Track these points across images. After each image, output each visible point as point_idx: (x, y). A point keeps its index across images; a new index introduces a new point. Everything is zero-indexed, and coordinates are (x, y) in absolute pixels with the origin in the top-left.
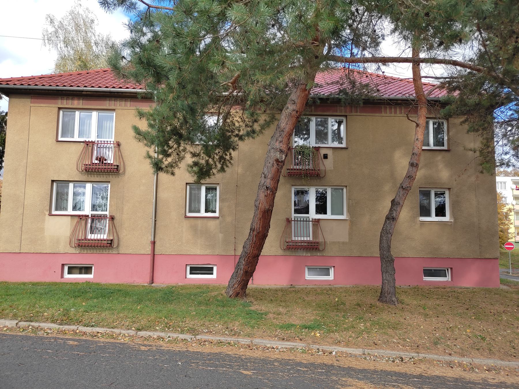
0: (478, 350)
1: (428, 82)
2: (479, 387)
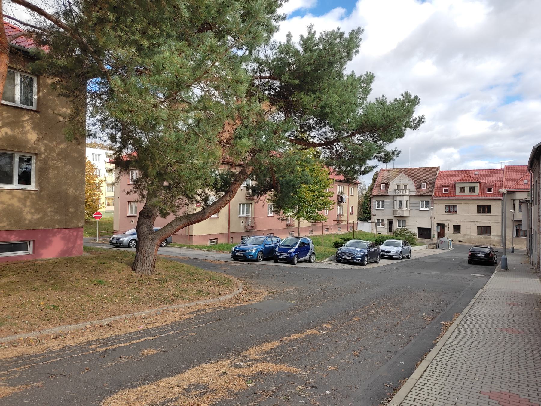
0: (48, 320)
1: (7, 21)
2: (41, 358)
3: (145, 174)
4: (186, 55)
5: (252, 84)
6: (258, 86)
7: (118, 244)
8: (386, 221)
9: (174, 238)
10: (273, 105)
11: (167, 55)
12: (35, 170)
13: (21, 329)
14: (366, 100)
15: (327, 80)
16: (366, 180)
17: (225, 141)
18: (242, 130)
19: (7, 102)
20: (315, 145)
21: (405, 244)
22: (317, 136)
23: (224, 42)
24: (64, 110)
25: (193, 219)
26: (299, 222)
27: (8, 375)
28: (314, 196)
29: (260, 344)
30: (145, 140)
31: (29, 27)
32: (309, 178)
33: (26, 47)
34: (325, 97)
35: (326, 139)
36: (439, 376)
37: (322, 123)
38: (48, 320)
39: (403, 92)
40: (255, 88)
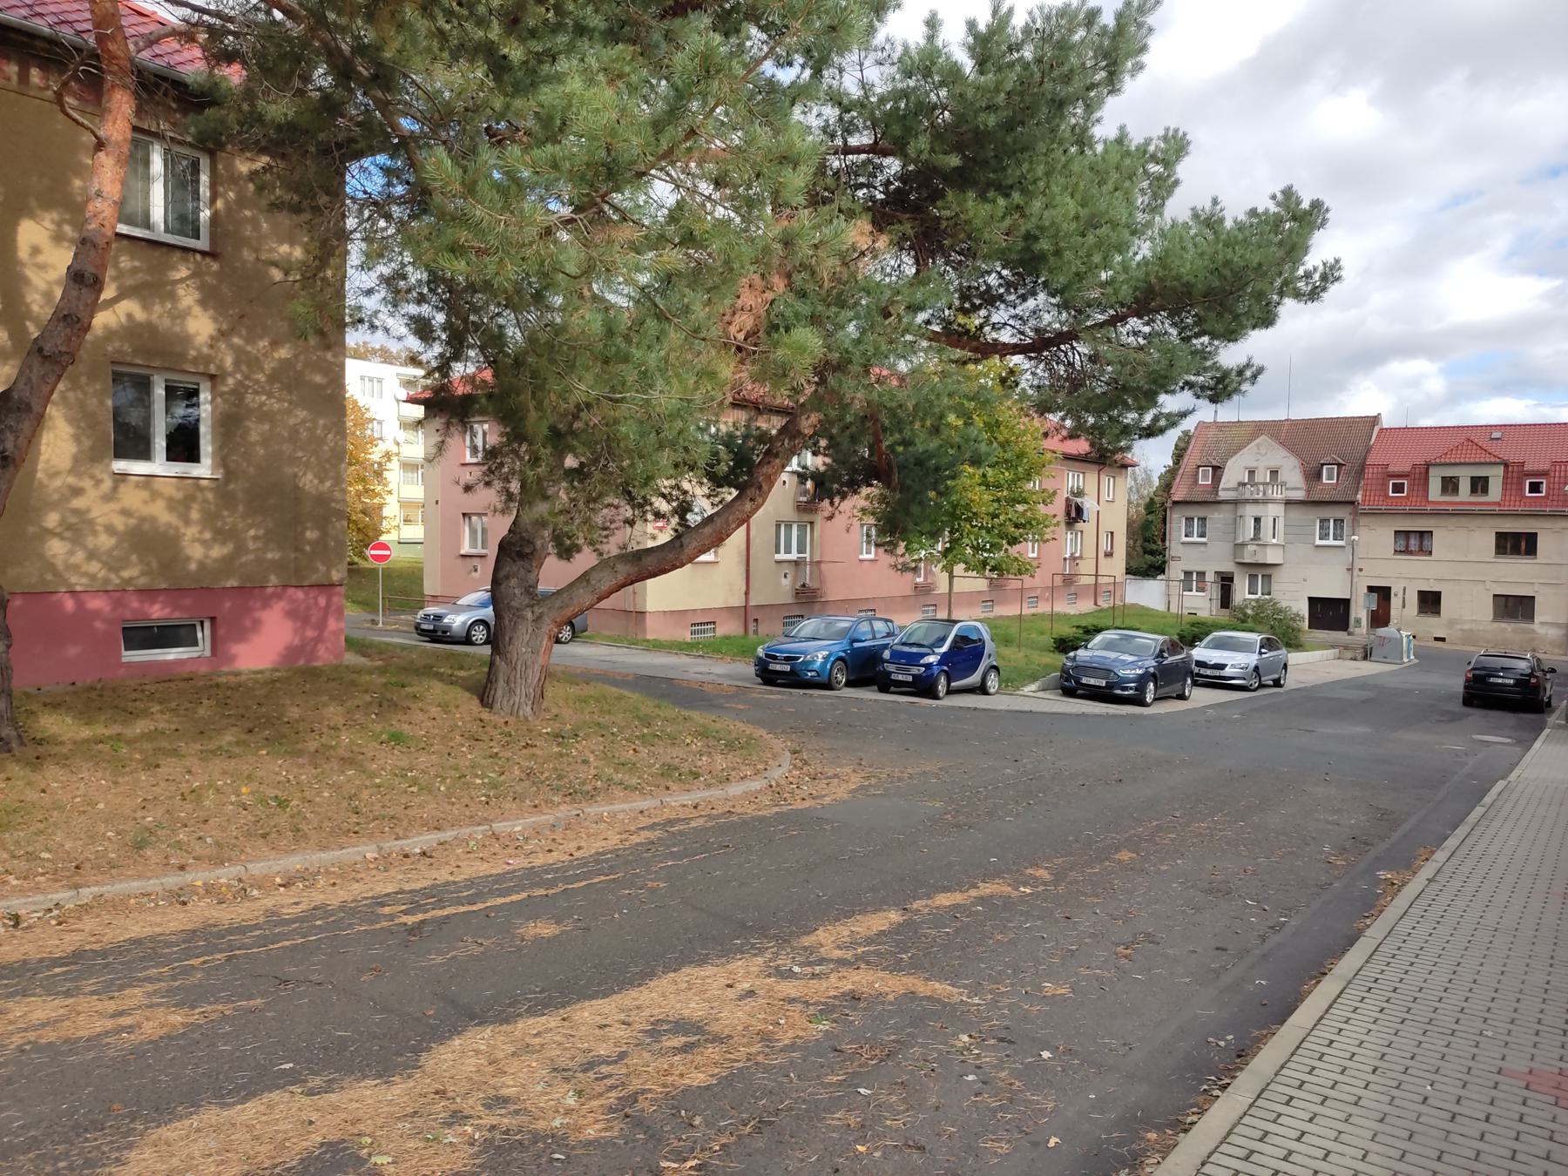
0: (264, 836)
3: (516, 433)
4: (629, 85)
5: (822, 168)
6: (837, 173)
7: (437, 634)
8: (1210, 577)
9: (592, 619)
10: (881, 230)
11: (575, 84)
12: (210, 423)
13: (194, 858)
14: (1161, 215)
15: (1045, 155)
16: (1152, 456)
17: (741, 336)
18: (790, 306)
19: (131, 228)
20: (1005, 350)
21: (1268, 644)
22: (1011, 322)
23: (738, 45)
24: (285, 249)
25: (649, 562)
26: (951, 577)
27: (174, 978)
28: (998, 500)
29: (845, 917)
30: (514, 333)
31: (189, 11)
32: (983, 448)
33: (179, 68)
34: (1037, 205)
35: (1037, 330)
36: (1374, 1022)
37: (1025, 285)
38: (264, 836)
39: (1277, 189)
40: (830, 181)
